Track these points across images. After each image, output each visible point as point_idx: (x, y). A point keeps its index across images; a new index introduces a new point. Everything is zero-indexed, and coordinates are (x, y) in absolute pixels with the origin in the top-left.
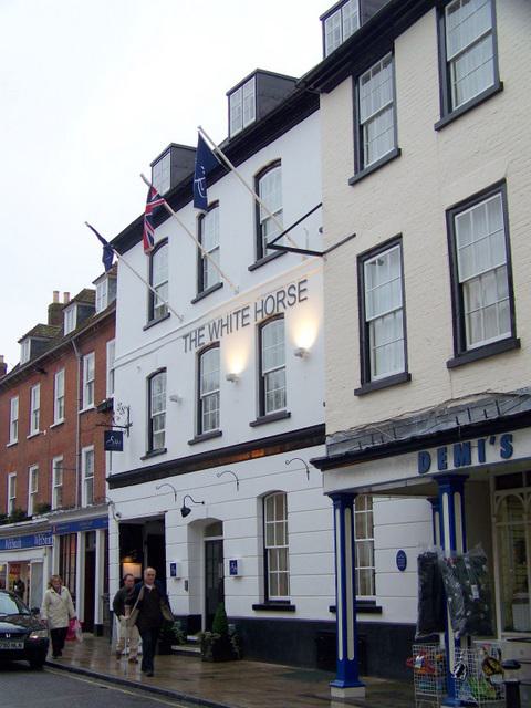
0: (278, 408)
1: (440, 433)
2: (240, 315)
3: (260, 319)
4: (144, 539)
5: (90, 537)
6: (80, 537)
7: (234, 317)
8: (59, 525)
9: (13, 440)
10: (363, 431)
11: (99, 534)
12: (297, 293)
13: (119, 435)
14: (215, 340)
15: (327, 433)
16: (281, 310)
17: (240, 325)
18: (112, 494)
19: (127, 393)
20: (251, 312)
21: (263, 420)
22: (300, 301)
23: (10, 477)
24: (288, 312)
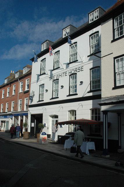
0: (98, 88)
1: (112, 102)
2: (65, 74)
3: (70, 74)
4: (38, 119)
5: (22, 117)
6: (19, 117)
7: (63, 74)
8: (14, 114)
9: (3, 98)
10: (115, 98)
11: (24, 117)
12: (81, 69)
13: (32, 97)
14: (57, 78)
15: (102, 97)
16: (76, 72)
17: (64, 75)
18: (30, 109)
19: (35, 89)
20: (68, 73)
21: (39, 101)
22: (81, 71)
23: (6, 104)
24: (78, 73)
